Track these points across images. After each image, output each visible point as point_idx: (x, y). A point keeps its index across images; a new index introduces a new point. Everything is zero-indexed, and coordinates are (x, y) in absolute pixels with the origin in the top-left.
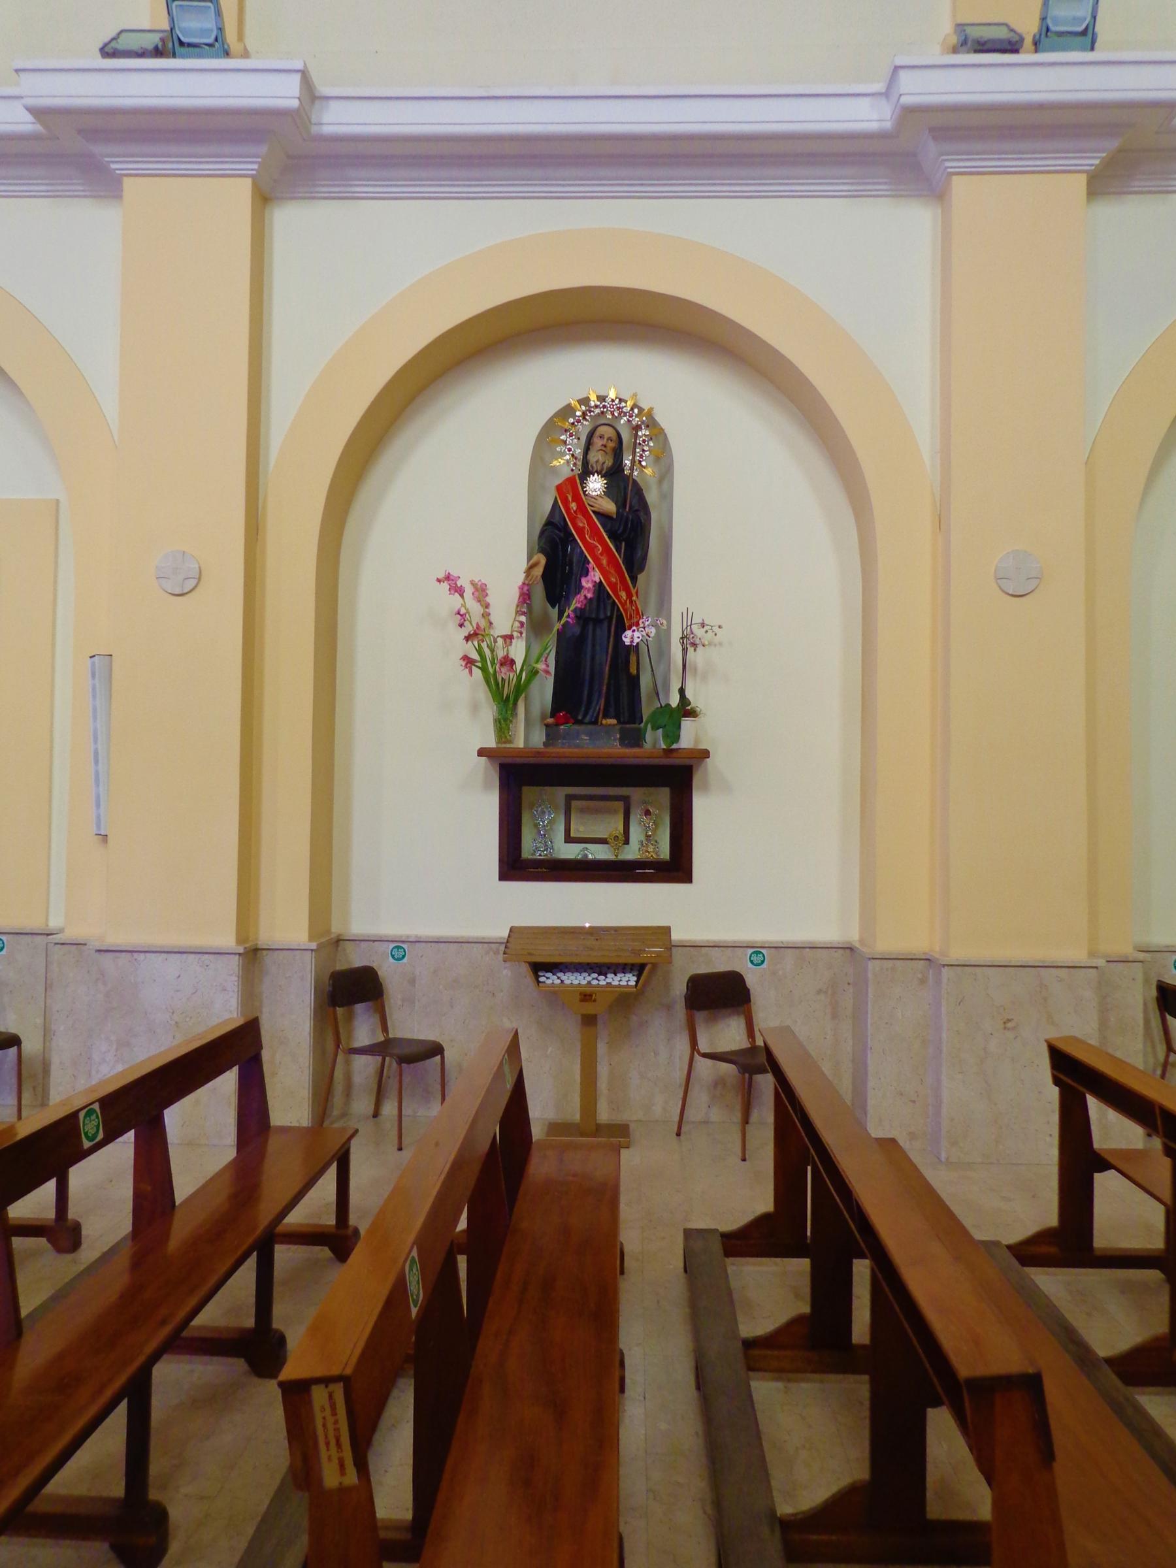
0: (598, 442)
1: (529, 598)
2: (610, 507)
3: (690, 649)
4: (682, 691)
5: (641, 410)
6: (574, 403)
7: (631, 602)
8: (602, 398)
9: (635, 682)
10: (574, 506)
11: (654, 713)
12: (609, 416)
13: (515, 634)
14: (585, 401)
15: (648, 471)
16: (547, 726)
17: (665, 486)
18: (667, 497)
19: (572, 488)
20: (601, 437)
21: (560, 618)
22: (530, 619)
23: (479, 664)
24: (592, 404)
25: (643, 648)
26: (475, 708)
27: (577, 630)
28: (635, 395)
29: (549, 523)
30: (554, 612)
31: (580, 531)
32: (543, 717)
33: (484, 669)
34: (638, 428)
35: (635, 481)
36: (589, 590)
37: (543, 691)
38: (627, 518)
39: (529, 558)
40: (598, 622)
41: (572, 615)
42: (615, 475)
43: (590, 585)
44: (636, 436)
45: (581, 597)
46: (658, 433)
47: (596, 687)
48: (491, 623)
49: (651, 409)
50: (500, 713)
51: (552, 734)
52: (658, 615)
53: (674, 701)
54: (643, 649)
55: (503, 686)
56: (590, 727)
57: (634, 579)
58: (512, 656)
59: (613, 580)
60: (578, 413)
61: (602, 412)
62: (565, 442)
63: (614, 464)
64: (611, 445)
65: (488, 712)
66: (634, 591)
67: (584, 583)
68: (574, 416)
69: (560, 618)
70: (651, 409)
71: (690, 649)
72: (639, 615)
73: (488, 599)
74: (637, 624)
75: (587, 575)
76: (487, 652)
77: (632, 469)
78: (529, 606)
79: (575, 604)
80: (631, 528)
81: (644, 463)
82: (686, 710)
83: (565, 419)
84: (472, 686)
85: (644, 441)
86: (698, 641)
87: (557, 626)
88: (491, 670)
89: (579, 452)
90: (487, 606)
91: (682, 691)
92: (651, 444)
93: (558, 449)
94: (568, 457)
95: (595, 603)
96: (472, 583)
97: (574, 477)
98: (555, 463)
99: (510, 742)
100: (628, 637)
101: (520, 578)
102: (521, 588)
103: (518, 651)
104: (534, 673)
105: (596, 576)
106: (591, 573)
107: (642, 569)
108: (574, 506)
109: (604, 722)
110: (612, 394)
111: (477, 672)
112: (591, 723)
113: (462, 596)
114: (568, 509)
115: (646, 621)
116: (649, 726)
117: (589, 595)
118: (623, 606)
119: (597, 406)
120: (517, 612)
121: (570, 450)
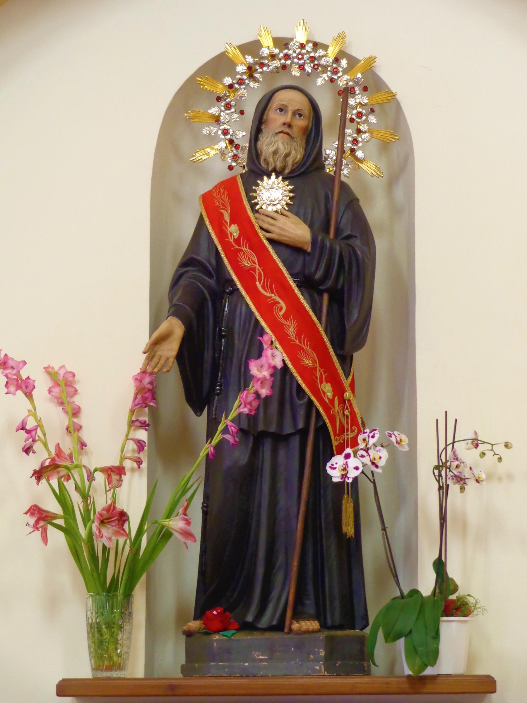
0: (276, 120)
1: (153, 398)
2: (298, 231)
3: (454, 488)
4: (440, 566)
5: (353, 61)
6: (234, 53)
7: (342, 401)
8: (282, 43)
9: (351, 548)
10: (234, 230)
11: (389, 608)
12: (296, 72)
13: (128, 464)
14: (251, 48)
15: (368, 167)
16: (189, 634)
17: (399, 193)
18: (403, 211)
19: (230, 200)
20: (282, 109)
21: (210, 435)
22: (155, 436)
23: (61, 522)
24: (265, 52)
25: (366, 487)
26: (52, 603)
27: (241, 456)
28: (342, 36)
29: (188, 262)
30: (201, 422)
31: (246, 275)
32: (181, 618)
33: (69, 531)
34: (347, 92)
35: (344, 186)
36: (263, 381)
37: (181, 569)
38: (332, 250)
39: (154, 325)
40: (280, 439)
41: (232, 429)
42: (307, 174)
43: (266, 373)
44: (345, 106)
45: (248, 395)
46: (387, 105)
47: (281, 559)
48: (83, 445)
49: (372, 60)
50: (100, 610)
51: (196, 655)
52: (394, 424)
53: (426, 584)
54: (366, 489)
55: (106, 561)
56: (268, 635)
57: (346, 360)
58: (121, 505)
59: (308, 362)
60: (241, 68)
61: (284, 67)
62: (217, 120)
63: (306, 156)
64: (301, 123)
65: (78, 610)
66: (346, 383)
67: (254, 369)
68: (232, 72)
69: (210, 435)
70: (372, 60)
71: (454, 488)
72: (357, 425)
73: (77, 400)
74: (354, 443)
75: (260, 356)
76: (76, 499)
77: (338, 164)
78: (154, 413)
79: (240, 406)
80: (340, 274)
81: (360, 154)
82: (449, 603)
83: (218, 77)
84: (46, 566)
85: (359, 115)
86: (467, 473)
87: (206, 449)
88: (83, 532)
89: (242, 136)
90: (76, 412)
91: (440, 566)
92: (373, 119)
93: (205, 131)
94: (222, 145)
95: (274, 407)
96: (48, 370)
97: (233, 180)
98: (199, 156)
99: (120, 667)
100: (336, 468)
101: (138, 361)
102: (138, 379)
103: (133, 496)
104: (166, 535)
105: (276, 356)
106: (268, 352)
107: (360, 339)
108: (234, 230)
109: (295, 626)
110: (301, 37)
111: (57, 537)
112: (271, 629)
113: (29, 396)
114: (222, 235)
115: (370, 438)
116: (380, 634)
117: (264, 392)
118: (327, 409)
119: (273, 57)
120: (132, 423)
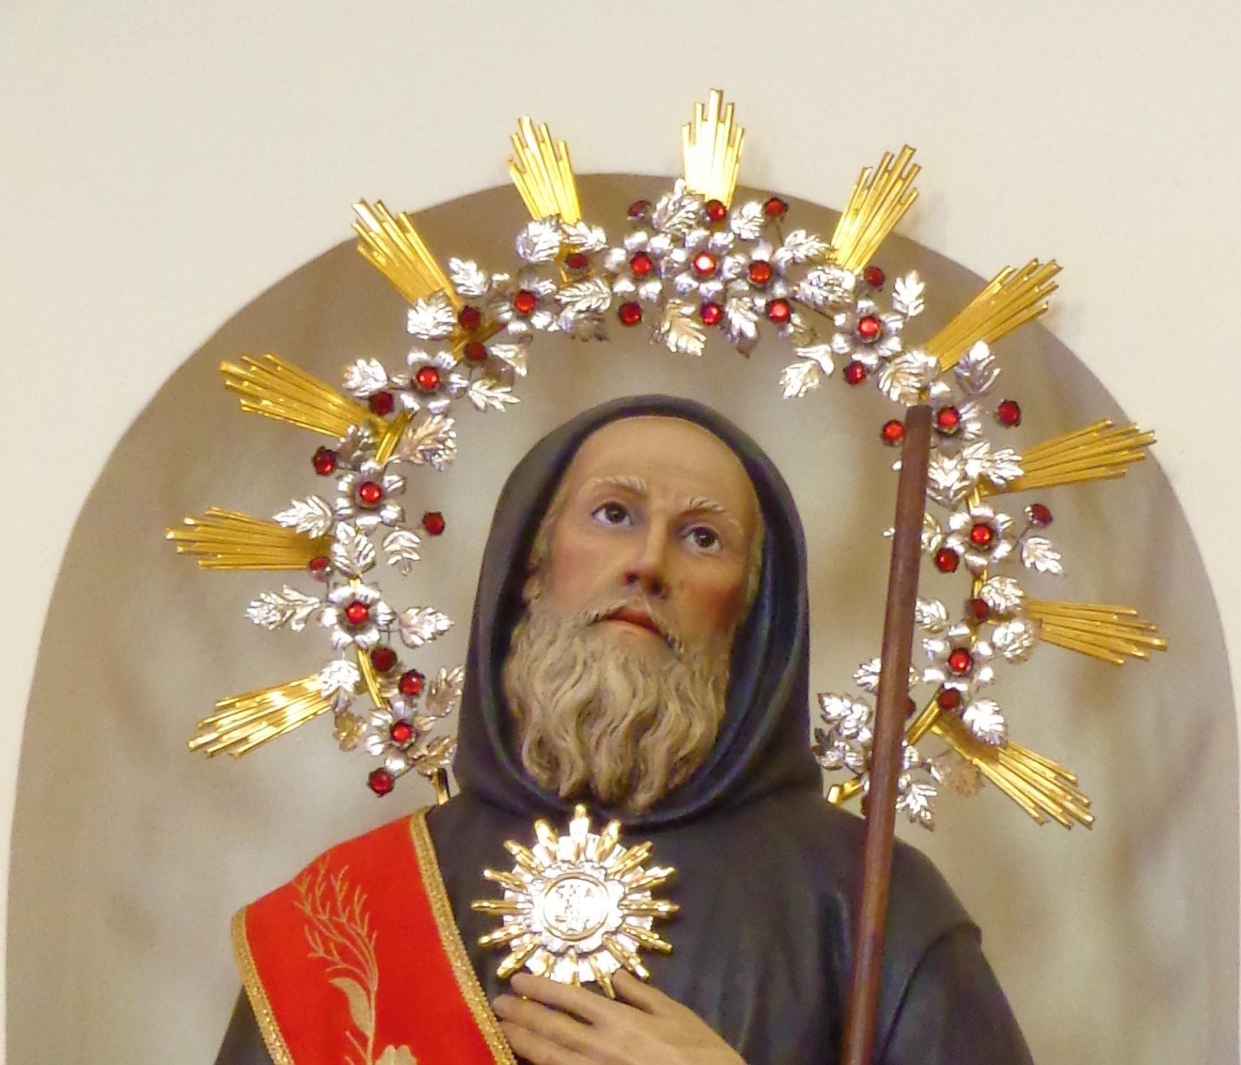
0: (592, 557)
5: (951, 286)
6: (398, 249)
8: (621, 200)
12: (685, 337)
15: (1023, 780)
24: (542, 241)
28: (898, 170)
35: (908, 868)
42: (730, 797)
44: (914, 493)
60: (428, 319)
61: (630, 311)
62: (317, 557)
63: (733, 729)
64: (708, 571)
68: (387, 334)
70: (1038, 278)
77: (882, 763)
81: (982, 718)
85: (982, 535)
89: (433, 631)
92: (1043, 555)
93: (261, 613)
94: (343, 674)
97: (392, 838)
110: (708, 171)
121: (356, 616)
